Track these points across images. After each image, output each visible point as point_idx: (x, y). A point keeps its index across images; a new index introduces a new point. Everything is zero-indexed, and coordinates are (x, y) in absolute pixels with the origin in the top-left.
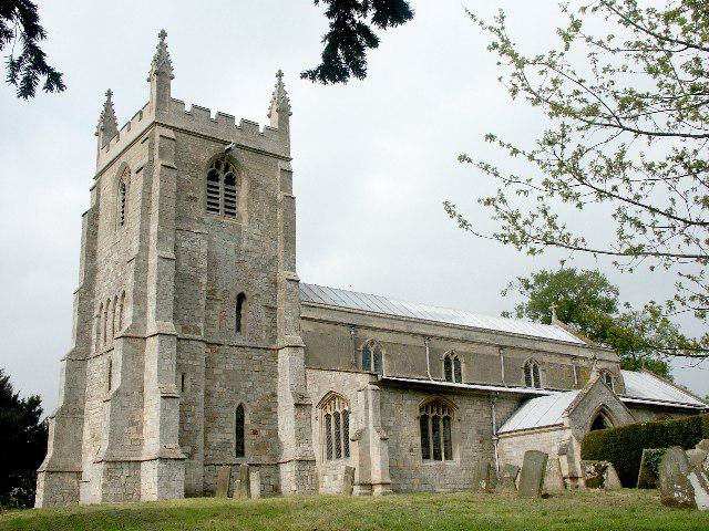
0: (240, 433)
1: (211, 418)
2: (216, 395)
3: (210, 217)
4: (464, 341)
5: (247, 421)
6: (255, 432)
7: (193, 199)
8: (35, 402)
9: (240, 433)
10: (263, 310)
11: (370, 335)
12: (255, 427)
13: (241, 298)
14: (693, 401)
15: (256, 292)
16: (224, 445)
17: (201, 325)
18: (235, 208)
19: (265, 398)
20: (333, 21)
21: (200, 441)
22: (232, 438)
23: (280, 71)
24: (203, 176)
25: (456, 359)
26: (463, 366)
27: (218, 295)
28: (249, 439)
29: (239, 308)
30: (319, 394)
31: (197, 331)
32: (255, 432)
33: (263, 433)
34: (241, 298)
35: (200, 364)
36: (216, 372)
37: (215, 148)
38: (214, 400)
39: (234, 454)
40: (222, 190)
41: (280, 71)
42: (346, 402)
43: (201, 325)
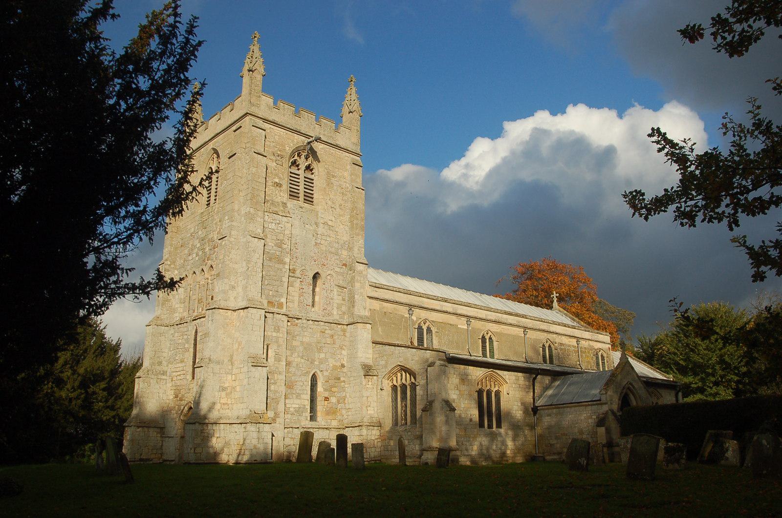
0: (313, 400)
1: (289, 385)
2: (294, 364)
3: (291, 204)
4: (495, 322)
5: (320, 388)
6: (327, 399)
7: (279, 185)
8: (118, 346)
9: (313, 400)
10: (336, 289)
11: (424, 314)
12: (326, 394)
13: (316, 276)
14: (511, 311)
15: (329, 272)
16: (299, 411)
17: (283, 300)
18: (313, 198)
19: (335, 368)
20: (84, 7)
21: (281, 407)
22: (307, 404)
23: (760, 106)
24: (287, 163)
25: (490, 338)
26: (495, 344)
27: (298, 274)
28: (320, 406)
29: (315, 286)
30: (386, 367)
31: (280, 305)
32: (327, 399)
33: (333, 400)
34: (316, 276)
35: (282, 335)
36: (295, 343)
37: (301, 140)
38: (292, 369)
39: (309, 418)
40: (302, 177)
41: (760, 106)
42: (124, 222)
43: (283, 300)
